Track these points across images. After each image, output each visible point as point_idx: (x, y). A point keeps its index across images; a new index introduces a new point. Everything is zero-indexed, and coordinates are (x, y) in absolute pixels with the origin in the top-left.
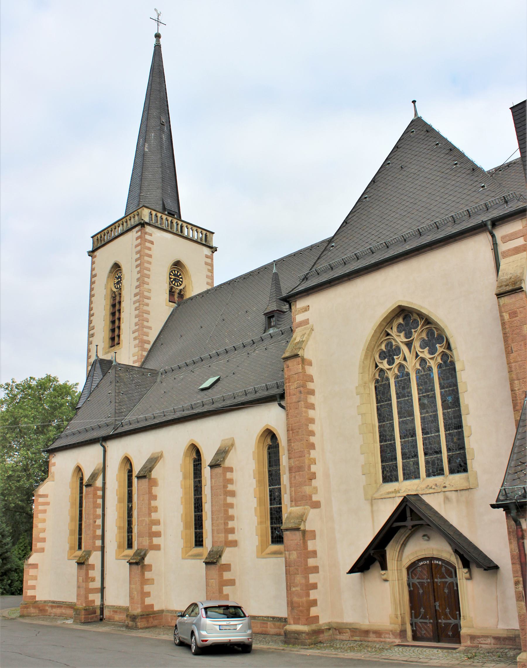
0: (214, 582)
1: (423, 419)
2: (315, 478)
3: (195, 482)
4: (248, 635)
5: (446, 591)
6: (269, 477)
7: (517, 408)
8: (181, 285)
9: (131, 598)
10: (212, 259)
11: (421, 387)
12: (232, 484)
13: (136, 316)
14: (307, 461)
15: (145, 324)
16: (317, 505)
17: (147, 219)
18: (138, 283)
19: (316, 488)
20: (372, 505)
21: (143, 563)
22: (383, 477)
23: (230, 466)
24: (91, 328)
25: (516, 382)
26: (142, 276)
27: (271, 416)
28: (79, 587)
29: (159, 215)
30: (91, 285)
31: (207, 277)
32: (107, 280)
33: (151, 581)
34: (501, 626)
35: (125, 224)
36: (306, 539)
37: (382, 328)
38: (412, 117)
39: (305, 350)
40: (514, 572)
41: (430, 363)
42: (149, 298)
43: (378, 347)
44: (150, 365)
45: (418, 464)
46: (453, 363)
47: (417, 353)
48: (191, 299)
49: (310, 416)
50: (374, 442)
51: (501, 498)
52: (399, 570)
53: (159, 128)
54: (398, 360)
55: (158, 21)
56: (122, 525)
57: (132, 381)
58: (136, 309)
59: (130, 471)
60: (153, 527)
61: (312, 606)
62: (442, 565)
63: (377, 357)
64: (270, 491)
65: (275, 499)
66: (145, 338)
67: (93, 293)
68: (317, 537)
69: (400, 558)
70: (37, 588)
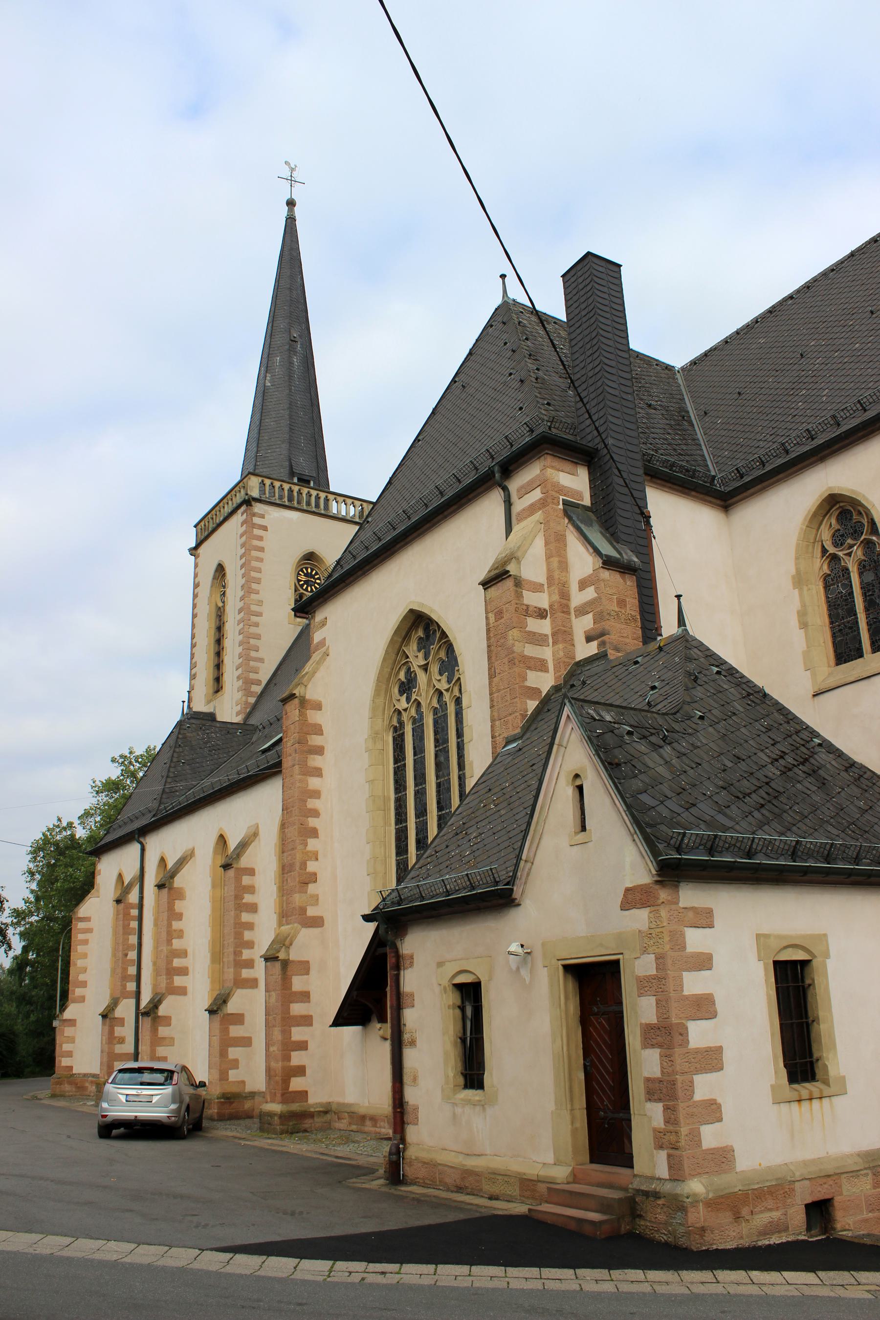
2: (315, 881)
4: (173, 1111)
12: (253, 893)
14: (299, 857)
15: (253, 654)
16: (317, 922)
17: (255, 494)
21: (156, 1013)
23: (249, 866)
26: (247, 581)
28: (102, 1052)
29: (286, 487)
32: (211, 591)
36: (289, 973)
37: (397, 646)
38: (498, 301)
39: (309, 686)
50: (386, 823)
53: (287, 347)
55: (292, 180)
57: (206, 743)
61: (295, 1076)
63: (396, 690)
66: (252, 676)
68: (312, 972)
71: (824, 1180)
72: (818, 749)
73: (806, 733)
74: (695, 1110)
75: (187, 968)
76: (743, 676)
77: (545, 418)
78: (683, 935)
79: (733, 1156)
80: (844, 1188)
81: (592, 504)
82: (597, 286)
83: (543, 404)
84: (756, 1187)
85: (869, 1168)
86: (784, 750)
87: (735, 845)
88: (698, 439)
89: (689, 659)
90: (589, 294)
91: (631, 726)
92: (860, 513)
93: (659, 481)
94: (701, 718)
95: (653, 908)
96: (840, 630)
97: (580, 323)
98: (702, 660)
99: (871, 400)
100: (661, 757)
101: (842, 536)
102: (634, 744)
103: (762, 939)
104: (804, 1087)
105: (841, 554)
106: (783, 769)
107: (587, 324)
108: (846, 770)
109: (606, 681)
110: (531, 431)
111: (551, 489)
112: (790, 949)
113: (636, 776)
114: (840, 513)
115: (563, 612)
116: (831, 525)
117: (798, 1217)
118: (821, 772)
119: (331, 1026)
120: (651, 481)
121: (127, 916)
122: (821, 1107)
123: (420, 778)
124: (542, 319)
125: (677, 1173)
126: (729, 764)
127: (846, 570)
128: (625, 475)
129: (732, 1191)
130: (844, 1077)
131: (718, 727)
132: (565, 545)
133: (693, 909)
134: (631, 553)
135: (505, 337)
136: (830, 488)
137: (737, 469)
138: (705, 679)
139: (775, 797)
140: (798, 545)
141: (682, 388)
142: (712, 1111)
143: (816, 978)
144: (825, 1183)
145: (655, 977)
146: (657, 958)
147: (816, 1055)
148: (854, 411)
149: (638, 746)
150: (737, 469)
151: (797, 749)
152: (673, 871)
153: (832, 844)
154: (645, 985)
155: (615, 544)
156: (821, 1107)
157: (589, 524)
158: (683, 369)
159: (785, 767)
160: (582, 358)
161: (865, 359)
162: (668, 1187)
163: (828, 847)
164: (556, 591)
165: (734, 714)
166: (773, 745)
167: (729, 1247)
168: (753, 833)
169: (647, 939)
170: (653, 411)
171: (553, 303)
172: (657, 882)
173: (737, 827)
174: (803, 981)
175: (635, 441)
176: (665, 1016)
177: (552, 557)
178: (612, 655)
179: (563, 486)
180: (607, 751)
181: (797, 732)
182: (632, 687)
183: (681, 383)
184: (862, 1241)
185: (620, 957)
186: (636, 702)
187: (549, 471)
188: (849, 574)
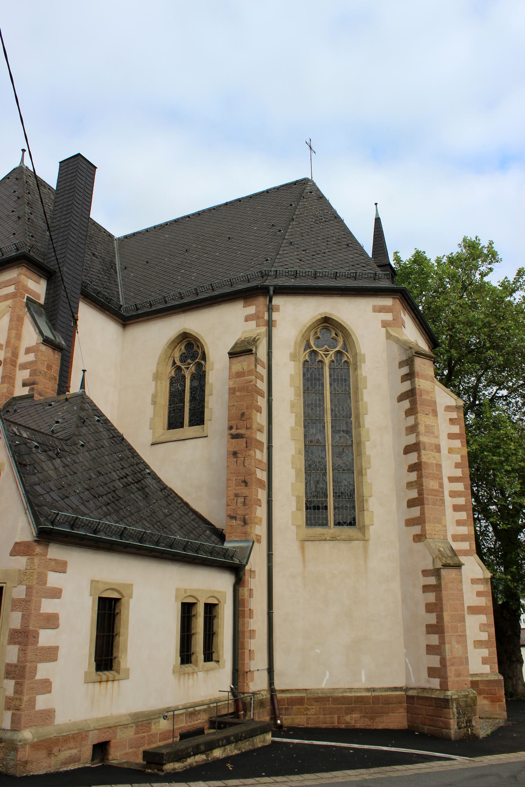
38: (17, 164)
71: (107, 730)
72: (147, 476)
73: (142, 465)
74: (35, 685)
76: (112, 426)
77: (28, 244)
78: (46, 576)
79: (54, 715)
80: (118, 734)
81: (45, 303)
82: (79, 175)
83: (29, 236)
84: (65, 734)
85: (134, 723)
86: (127, 473)
87: (87, 525)
88: (118, 282)
89: (82, 409)
90: (74, 178)
91: (38, 443)
92: (198, 347)
93: (89, 300)
94: (82, 446)
95: (30, 557)
96: (174, 410)
97: (63, 193)
98: (90, 411)
99: (218, 286)
100: (53, 465)
101: (186, 357)
102: (38, 454)
103: (94, 583)
104: (104, 674)
105: (183, 367)
106: (125, 484)
107: (68, 196)
108: (161, 491)
109: (29, 412)
110: (17, 249)
111: (21, 289)
112: (110, 591)
113: (35, 474)
114: (188, 344)
115: (12, 365)
116: (181, 349)
117: (87, 752)
118: (146, 489)
120: (84, 299)
122: (113, 686)
124: (40, 183)
125: (16, 726)
126: (94, 476)
127: (184, 377)
128: (68, 291)
129: (49, 737)
130: (129, 669)
131: (92, 453)
132: (22, 324)
133: (55, 560)
134: (62, 339)
135: (15, 187)
136: (185, 328)
137: (136, 305)
138: (89, 423)
139: (117, 500)
140: (160, 356)
141: (116, 250)
142: (46, 686)
143: (122, 609)
144: (107, 732)
145: (24, 600)
146: (27, 588)
147: (115, 655)
148: (208, 289)
149: (40, 456)
150: (136, 305)
151: (135, 473)
152: (46, 536)
153: (145, 532)
154: (16, 604)
155: (53, 331)
156: (113, 686)
157: (40, 315)
158: (119, 239)
159: (126, 483)
160: (60, 214)
161: (220, 262)
162: (8, 735)
163: (142, 533)
164: (10, 351)
165: (103, 447)
166: (122, 469)
167: (41, 773)
168: (100, 519)
169: (23, 576)
170: (95, 258)
171: (50, 176)
172: (36, 541)
173: (91, 514)
174: (114, 611)
175: (80, 273)
176: (26, 625)
177: (12, 329)
178: (37, 397)
179: (29, 288)
180: (20, 455)
181: (137, 464)
182: (44, 419)
183: (116, 247)
184: (122, 766)
185: (4, 585)
186: (45, 429)
187: (23, 277)
188: (185, 379)
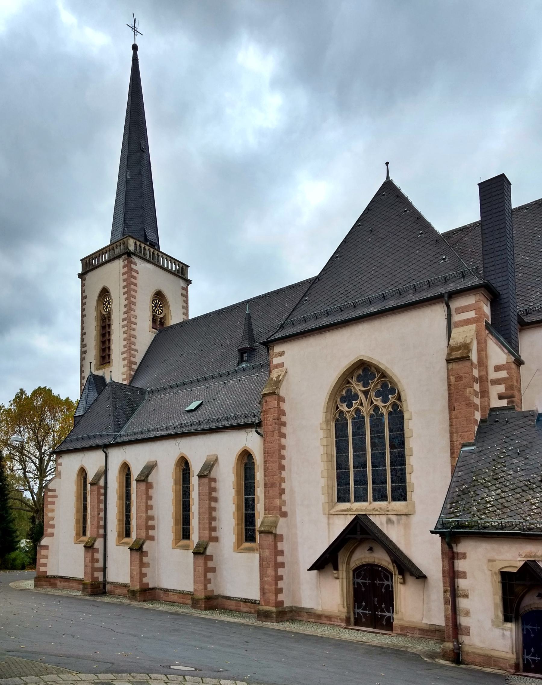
0: (201, 569)
1: (372, 454)
3: (183, 487)
5: (383, 591)
6: (245, 489)
7: (454, 455)
8: (161, 313)
9: (132, 577)
10: (187, 291)
11: (373, 429)
13: (125, 340)
16: (284, 515)
17: (132, 248)
18: (126, 309)
19: (284, 501)
20: (328, 518)
22: (338, 497)
24: (83, 345)
25: (455, 434)
27: (251, 441)
28: (86, 566)
29: (143, 245)
30: (82, 306)
31: (183, 307)
33: (147, 565)
34: (425, 621)
35: (111, 251)
37: (345, 377)
38: (384, 179)
39: (281, 389)
40: (444, 583)
41: (382, 410)
42: (135, 324)
43: (340, 392)
44: (138, 384)
45: (367, 490)
46: (401, 412)
47: (372, 400)
48: (172, 327)
49: (282, 444)
50: (333, 469)
51: (439, 527)
52: (347, 571)
54: (355, 404)
56: (121, 518)
58: (124, 333)
59: (85, 478)
60: (150, 522)
61: (279, 593)
62: (381, 571)
63: (339, 400)
64: (246, 500)
65: (249, 506)
66: (133, 359)
67: (84, 313)
68: (284, 540)
69: (348, 563)
70: (48, 565)
75: (154, 526)
119: (308, 570)
121: (99, 493)
123: (359, 448)
